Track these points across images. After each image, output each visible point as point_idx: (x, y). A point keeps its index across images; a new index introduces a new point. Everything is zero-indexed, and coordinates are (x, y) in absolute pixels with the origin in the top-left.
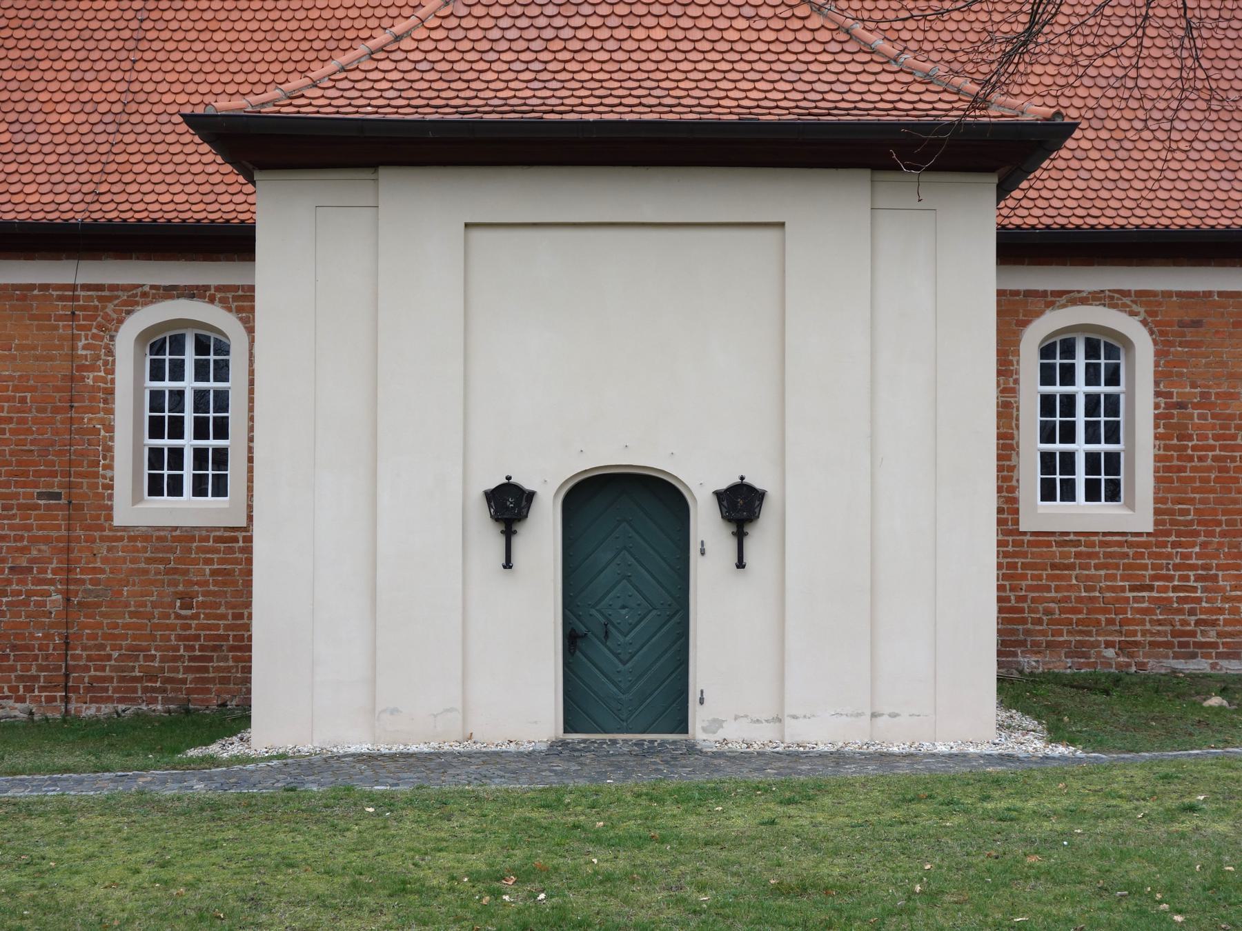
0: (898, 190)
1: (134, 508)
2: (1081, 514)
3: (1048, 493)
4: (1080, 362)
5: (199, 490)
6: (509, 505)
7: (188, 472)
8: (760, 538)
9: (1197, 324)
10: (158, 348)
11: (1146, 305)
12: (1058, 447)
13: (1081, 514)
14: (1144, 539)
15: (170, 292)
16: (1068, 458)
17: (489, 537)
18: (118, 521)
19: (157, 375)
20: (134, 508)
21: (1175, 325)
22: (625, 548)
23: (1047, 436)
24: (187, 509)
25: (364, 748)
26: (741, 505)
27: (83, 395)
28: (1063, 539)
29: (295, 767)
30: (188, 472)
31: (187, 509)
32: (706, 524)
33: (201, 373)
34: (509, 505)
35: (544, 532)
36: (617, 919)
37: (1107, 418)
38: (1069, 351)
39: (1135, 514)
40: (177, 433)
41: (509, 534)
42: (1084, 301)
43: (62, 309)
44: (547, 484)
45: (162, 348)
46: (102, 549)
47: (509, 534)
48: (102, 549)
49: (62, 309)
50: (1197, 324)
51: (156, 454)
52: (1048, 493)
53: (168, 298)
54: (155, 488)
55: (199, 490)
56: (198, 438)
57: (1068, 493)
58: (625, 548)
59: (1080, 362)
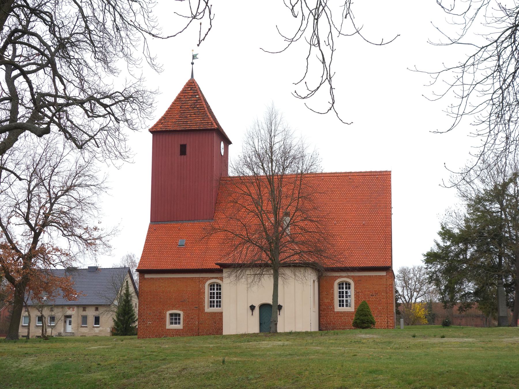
1: (208, 309)
3: (340, 306)
4: (344, 286)
5: (217, 306)
6: (252, 308)
7: (215, 304)
9: (360, 280)
10: (211, 286)
11: (353, 278)
12: (341, 299)
13: (345, 309)
15: (213, 278)
18: (182, 328)
19: (211, 290)
20: (208, 309)
21: (358, 281)
22: (268, 312)
23: (340, 297)
24: (215, 309)
25: (235, 333)
27: (201, 293)
28: (341, 313)
30: (215, 304)
31: (215, 309)
33: (217, 289)
34: (252, 308)
35: (257, 311)
37: (212, 296)
38: (214, 286)
40: (214, 298)
41: (252, 311)
43: (198, 280)
44: (257, 305)
45: (212, 286)
46: (203, 315)
47: (252, 311)
48: (203, 315)
49: (198, 280)
50: (360, 280)
52: (340, 306)
53: (212, 279)
54: (211, 307)
55: (217, 306)
56: (217, 297)
57: (214, 306)
58: (268, 312)
59: (344, 286)
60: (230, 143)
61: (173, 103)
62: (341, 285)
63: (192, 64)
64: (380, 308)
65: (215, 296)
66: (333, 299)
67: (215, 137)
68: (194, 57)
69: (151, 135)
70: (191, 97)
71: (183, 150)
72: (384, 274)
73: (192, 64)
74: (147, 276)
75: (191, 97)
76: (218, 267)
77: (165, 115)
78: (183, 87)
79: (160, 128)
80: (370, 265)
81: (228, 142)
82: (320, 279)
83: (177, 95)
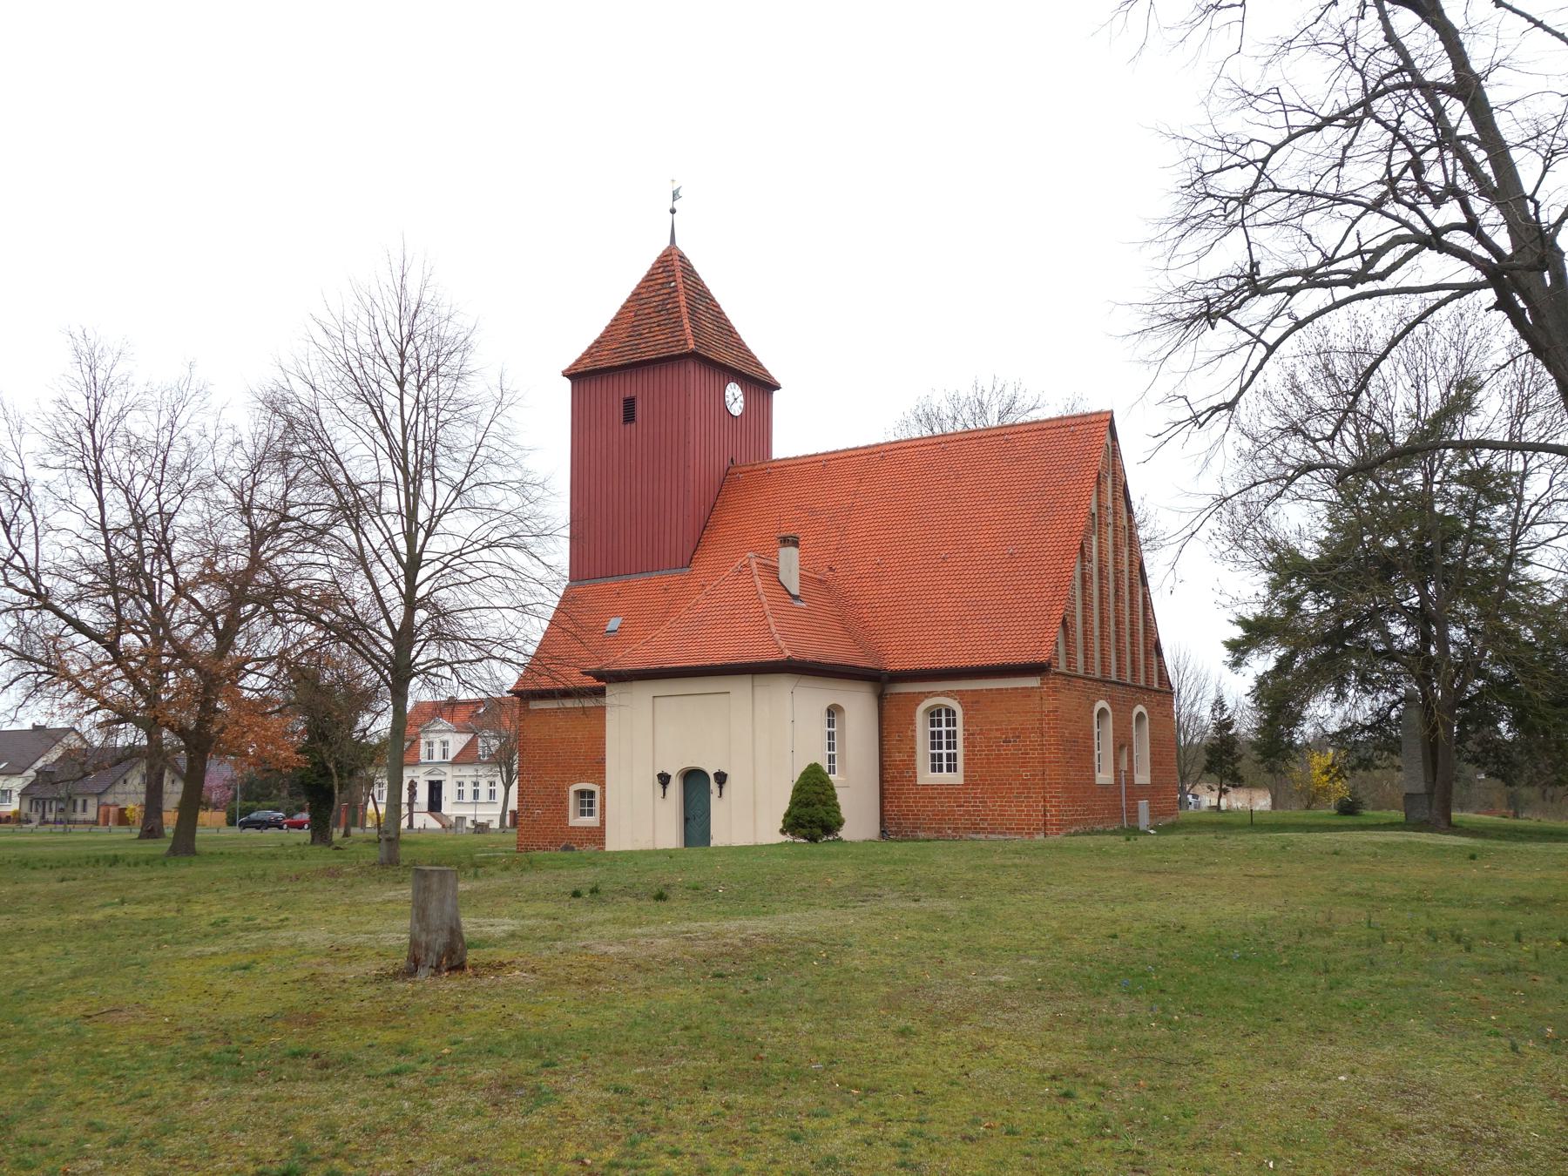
0: (761, 680)
2: (945, 777)
4: (944, 718)
5: (949, 770)
6: (664, 779)
8: (726, 788)
11: (959, 695)
13: (945, 777)
14: (405, 810)
16: (940, 755)
17: (659, 788)
21: (971, 702)
22: (697, 788)
26: (721, 778)
29: (716, 848)
32: (714, 786)
34: (664, 779)
35: (675, 786)
36: (727, 908)
39: (957, 778)
42: (938, 695)
44: (674, 771)
51: (933, 733)
52: (933, 770)
55: (949, 770)
57: (941, 770)
58: (697, 788)
59: (944, 718)
60: (770, 386)
61: (623, 307)
62: (934, 714)
63: (673, 211)
64: (1026, 775)
65: (944, 740)
66: (913, 752)
67: (695, 376)
68: (675, 196)
69: (567, 383)
70: (671, 290)
71: (629, 408)
72: (1033, 682)
73: (673, 211)
74: (536, 705)
75: (671, 290)
76: (591, 682)
77: (602, 336)
78: (648, 267)
79: (589, 365)
80: (997, 659)
81: (761, 386)
82: (881, 698)
83: (633, 287)
